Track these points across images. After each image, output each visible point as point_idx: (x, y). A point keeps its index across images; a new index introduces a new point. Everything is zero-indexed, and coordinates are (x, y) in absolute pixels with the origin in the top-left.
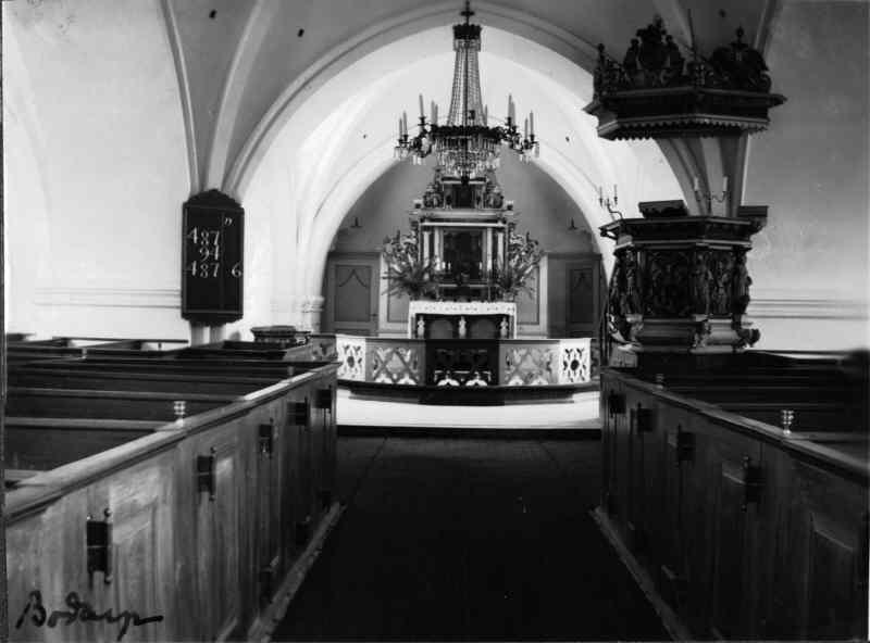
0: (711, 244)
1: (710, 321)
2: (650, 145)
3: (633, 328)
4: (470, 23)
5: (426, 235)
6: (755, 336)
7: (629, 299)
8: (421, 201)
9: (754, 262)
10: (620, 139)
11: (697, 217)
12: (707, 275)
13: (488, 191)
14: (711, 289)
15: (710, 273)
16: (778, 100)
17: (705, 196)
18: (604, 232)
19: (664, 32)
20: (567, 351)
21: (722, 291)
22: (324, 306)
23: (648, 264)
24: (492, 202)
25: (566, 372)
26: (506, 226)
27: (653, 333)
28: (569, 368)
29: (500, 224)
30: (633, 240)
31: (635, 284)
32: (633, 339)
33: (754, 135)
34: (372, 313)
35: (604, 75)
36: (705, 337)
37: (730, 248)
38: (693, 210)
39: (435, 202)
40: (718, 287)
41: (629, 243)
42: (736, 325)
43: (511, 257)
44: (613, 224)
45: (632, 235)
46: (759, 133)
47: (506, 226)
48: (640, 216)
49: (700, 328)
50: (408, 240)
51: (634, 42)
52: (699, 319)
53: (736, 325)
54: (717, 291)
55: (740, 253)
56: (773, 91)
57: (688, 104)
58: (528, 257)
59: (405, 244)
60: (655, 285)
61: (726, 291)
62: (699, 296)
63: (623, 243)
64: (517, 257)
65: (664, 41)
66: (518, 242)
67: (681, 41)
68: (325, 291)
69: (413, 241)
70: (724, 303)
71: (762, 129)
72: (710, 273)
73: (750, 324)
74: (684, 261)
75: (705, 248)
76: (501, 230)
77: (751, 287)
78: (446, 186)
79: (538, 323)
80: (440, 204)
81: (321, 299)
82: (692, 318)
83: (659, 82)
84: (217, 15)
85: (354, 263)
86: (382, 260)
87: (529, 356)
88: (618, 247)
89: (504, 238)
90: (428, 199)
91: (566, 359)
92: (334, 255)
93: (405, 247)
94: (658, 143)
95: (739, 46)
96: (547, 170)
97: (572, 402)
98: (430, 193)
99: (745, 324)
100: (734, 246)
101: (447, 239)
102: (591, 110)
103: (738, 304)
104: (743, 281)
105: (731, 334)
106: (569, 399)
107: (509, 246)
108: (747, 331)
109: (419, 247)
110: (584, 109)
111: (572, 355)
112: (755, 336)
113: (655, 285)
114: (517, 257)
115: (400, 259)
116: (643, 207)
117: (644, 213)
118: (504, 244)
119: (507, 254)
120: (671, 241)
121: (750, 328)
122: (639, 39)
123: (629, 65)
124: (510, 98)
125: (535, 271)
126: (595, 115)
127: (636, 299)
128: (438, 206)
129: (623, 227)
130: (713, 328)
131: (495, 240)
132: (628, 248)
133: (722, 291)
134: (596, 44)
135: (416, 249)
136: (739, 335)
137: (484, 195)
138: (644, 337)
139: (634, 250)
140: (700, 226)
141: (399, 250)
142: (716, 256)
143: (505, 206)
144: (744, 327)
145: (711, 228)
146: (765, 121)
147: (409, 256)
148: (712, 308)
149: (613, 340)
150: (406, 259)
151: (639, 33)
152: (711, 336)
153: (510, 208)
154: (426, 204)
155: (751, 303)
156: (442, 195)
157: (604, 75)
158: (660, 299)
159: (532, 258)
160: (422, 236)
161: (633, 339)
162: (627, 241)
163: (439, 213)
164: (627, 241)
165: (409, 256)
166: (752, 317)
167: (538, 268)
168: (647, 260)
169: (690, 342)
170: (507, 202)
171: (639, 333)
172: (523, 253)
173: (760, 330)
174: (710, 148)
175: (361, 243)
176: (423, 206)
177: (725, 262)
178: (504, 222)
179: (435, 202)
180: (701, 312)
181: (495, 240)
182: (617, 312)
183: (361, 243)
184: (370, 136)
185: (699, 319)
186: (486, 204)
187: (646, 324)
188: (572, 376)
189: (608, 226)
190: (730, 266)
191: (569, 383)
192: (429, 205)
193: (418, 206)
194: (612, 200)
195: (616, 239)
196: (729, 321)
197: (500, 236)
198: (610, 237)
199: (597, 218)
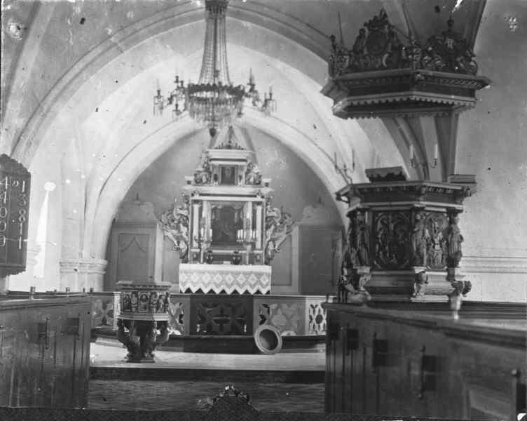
0: (427, 206)
1: (427, 273)
2: (376, 123)
3: (361, 279)
4: (13, 158)
5: (196, 207)
6: (466, 288)
7: (359, 254)
8: (192, 178)
9: (463, 224)
10: (352, 118)
11: (414, 182)
12: (424, 233)
13: (249, 171)
14: (428, 245)
15: (427, 231)
16: (483, 83)
17: (422, 163)
18: (339, 198)
19: (387, 22)
20: (312, 306)
21: (437, 247)
22: (107, 269)
23: (375, 223)
24: (252, 180)
25: (312, 325)
26: (264, 200)
27: (384, 283)
28: (314, 321)
29: (259, 199)
30: (361, 202)
31: (363, 240)
32: (362, 289)
33: (464, 112)
34: (149, 275)
35: (336, 60)
36: (423, 286)
37: (444, 210)
38: (410, 174)
39: (204, 180)
40: (435, 244)
41: (359, 205)
42: (450, 277)
43: (268, 227)
44: (345, 188)
45: (361, 198)
46: (468, 111)
47: (264, 200)
48: (367, 181)
49: (418, 279)
50: (181, 212)
51: (362, 31)
52: (418, 270)
53: (450, 277)
54: (434, 247)
55: (453, 213)
56: (480, 74)
57: (406, 83)
58: (283, 227)
59: (178, 215)
60: (380, 241)
61: (441, 247)
62: (418, 249)
63: (353, 205)
64: (273, 227)
65: (386, 30)
66: (274, 214)
67: (401, 32)
68: (108, 255)
69: (184, 212)
70: (440, 257)
71: (470, 107)
72: (427, 231)
73: (463, 276)
74: (407, 221)
75: (422, 209)
76: (259, 203)
77: (462, 244)
78: (214, 166)
79: (290, 285)
80: (208, 181)
81: (105, 262)
82: (413, 270)
83: (382, 65)
84: (86, 22)
85: (140, 231)
86: (158, 230)
87: (279, 310)
88: (351, 209)
89: (263, 210)
90: (198, 176)
91: (312, 313)
92: (115, 224)
93: (177, 218)
94: (383, 120)
95: (448, 33)
96: (321, 176)
97: (316, 351)
98: (199, 172)
99: (458, 276)
100: (447, 208)
101: (214, 211)
102: (327, 93)
103: (452, 261)
104: (455, 239)
105: (447, 286)
106: (314, 349)
107: (267, 218)
108: (460, 282)
109: (190, 217)
110: (322, 92)
111: (317, 309)
112: (466, 288)
113: (380, 241)
114: (273, 227)
115: (173, 228)
116: (370, 173)
117: (371, 178)
118: (262, 213)
119: (265, 224)
120: (394, 203)
121: (463, 280)
122: (366, 29)
123: (356, 51)
124: (251, 71)
125: (289, 239)
126: (331, 98)
127: (364, 254)
128: (206, 183)
129: (355, 191)
130: (429, 280)
131: (254, 212)
132: (358, 209)
133: (437, 247)
134: (329, 36)
135: (188, 219)
136: (453, 285)
137: (246, 174)
138: (371, 287)
139: (363, 211)
140: (414, 191)
141: (173, 221)
142: (432, 216)
143: (263, 184)
144: (457, 279)
145: (427, 192)
146: (473, 99)
147: (181, 225)
148: (429, 260)
149: (348, 291)
150: (178, 228)
151: (365, 25)
152: (428, 285)
153: (267, 185)
154: (196, 181)
155: (462, 259)
156: (210, 173)
157: (336, 60)
158: (384, 254)
159: (286, 228)
160: (193, 208)
161: (362, 289)
162: (357, 204)
163: (205, 189)
164: (357, 204)
165: (181, 225)
166: (463, 271)
167: (290, 236)
168: (373, 218)
169: (410, 292)
170: (264, 180)
171: (368, 282)
172: (278, 224)
173: (472, 283)
174: (427, 124)
175: (146, 211)
176: (193, 183)
177: (440, 221)
178: (263, 197)
179: (204, 180)
180: (421, 264)
181: (254, 212)
182: (350, 266)
183: (146, 211)
184: (148, 120)
185: (418, 270)
186: (248, 182)
187: (373, 276)
188: (317, 329)
189: (342, 190)
190: (445, 225)
191: (314, 334)
192: (198, 182)
193: (189, 183)
194: (349, 166)
195: (348, 202)
196: (446, 274)
197: (259, 209)
198: (344, 201)
199: (335, 184)
